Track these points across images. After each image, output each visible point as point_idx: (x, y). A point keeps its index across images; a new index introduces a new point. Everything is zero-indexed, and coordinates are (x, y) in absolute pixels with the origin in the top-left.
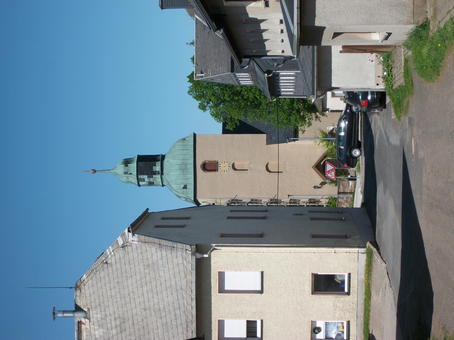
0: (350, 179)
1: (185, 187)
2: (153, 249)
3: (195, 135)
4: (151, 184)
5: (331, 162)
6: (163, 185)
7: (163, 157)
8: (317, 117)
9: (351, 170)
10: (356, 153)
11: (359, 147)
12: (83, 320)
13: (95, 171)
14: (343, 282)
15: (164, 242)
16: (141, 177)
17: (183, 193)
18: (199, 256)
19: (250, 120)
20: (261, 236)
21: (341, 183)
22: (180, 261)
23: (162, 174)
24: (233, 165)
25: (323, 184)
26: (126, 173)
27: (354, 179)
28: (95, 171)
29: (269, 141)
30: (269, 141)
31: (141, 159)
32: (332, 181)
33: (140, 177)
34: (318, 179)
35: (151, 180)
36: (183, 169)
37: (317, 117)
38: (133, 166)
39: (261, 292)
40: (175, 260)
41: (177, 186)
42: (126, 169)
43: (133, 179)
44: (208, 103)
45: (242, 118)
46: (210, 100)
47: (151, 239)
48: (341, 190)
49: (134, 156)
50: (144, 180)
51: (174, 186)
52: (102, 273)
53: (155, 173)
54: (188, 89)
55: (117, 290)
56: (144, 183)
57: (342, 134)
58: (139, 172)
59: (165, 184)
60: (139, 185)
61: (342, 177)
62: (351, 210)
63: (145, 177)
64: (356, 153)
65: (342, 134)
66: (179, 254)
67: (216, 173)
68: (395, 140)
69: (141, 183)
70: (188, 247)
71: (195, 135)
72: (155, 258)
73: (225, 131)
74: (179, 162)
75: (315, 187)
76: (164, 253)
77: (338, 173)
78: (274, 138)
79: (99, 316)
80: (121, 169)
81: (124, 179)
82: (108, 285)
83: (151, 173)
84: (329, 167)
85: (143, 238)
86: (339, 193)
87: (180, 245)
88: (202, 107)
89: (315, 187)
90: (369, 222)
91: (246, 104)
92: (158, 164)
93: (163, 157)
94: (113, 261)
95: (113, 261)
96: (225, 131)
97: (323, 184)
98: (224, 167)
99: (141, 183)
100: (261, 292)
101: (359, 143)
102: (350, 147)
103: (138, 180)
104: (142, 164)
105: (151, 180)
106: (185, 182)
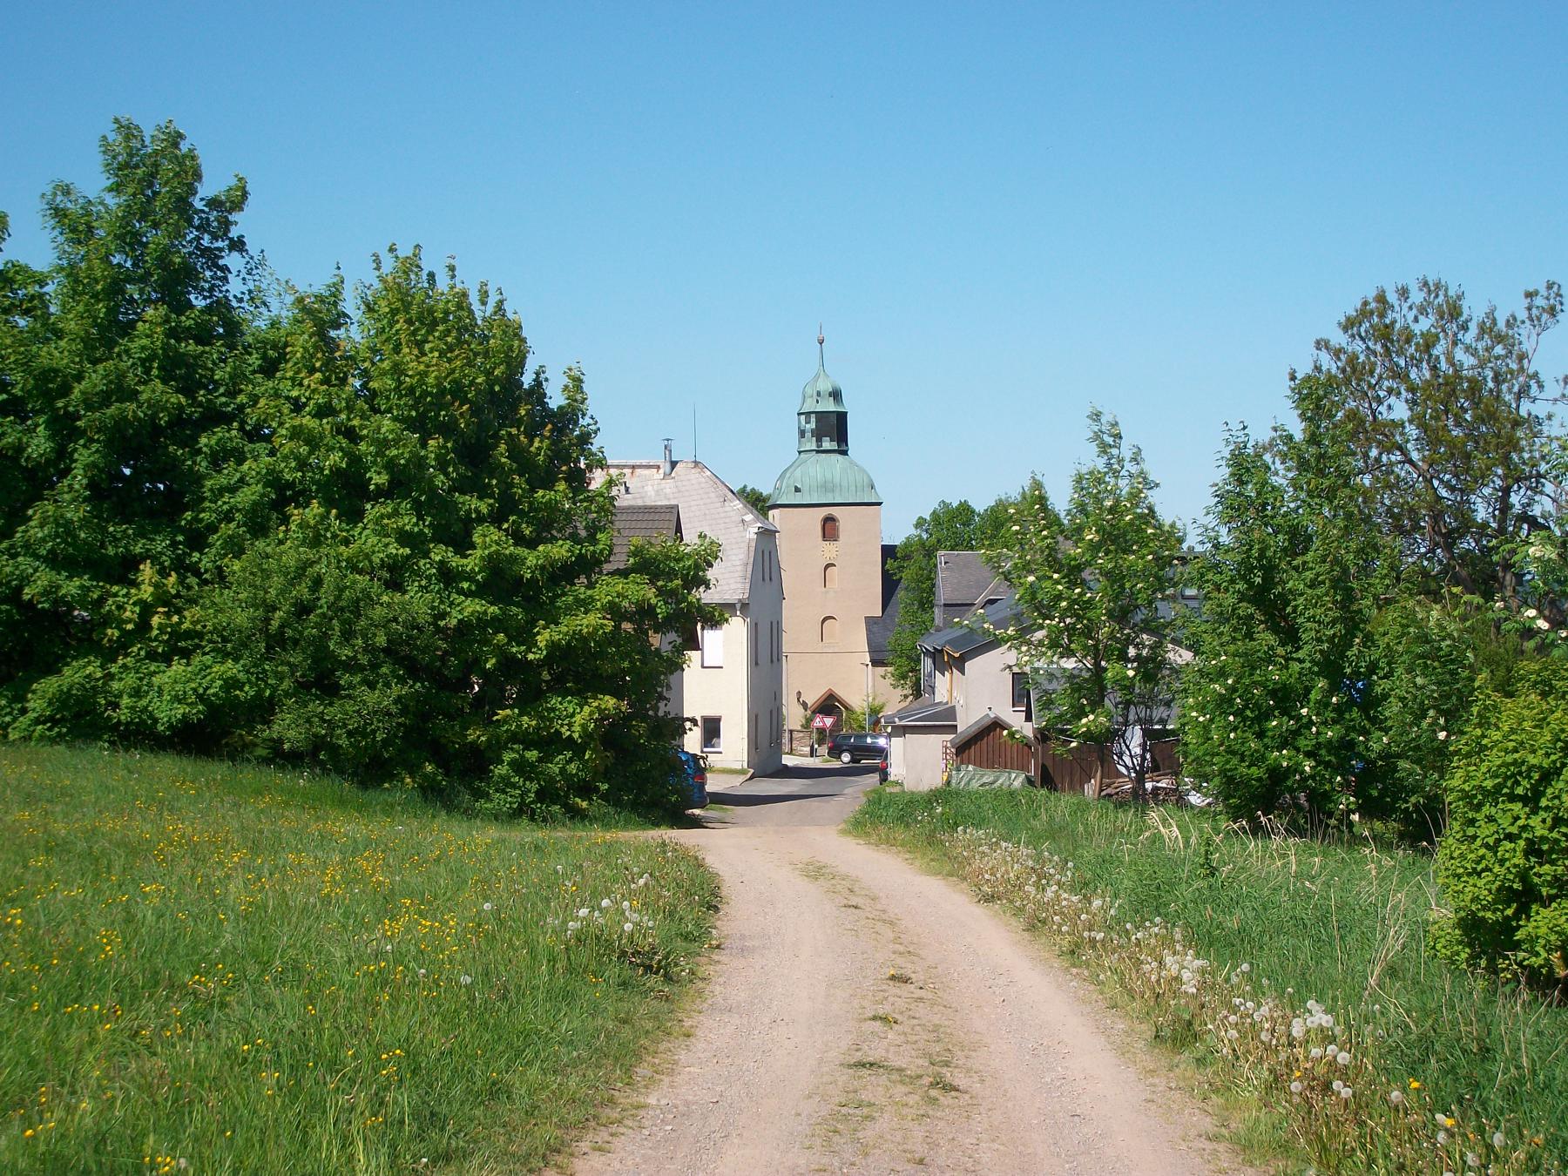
0: (812, 747)
1: (797, 490)
2: (742, 556)
3: (879, 504)
4: (802, 433)
5: (837, 725)
6: (800, 452)
7: (845, 453)
8: (906, 697)
9: (824, 750)
10: (846, 757)
11: (853, 761)
12: (661, 471)
13: (821, 343)
14: (713, 746)
15: (750, 568)
16: (813, 419)
17: (788, 487)
18: (738, 606)
19: (900, 594)
20: (757, 664)
21: (808, 734)
22: (733, 586)
23: (818, 452)
24: (834, 565)
25: (805, 705)
26: (819, 394)
27: (812, 753)
28: (821, 343)
29: (870, 621)
30: (870, 621)
31: (842, 417)
32: (809, 721)
33: (813, 416)
34: (812, 698)
35: (808, 435)
36: (826, 487)
37: (906, 697)
38: (829, 405)
39: (703, 667)
40: (732, 581)
41: (797, 477)
42: (824, 393)
43: (810, 406)
44: (927, 531)
45: (904, 583)
46: (931, 535)
47: (752, 554)
48: (795, 735)
49: (849, 405)
50: (808, 422)
51: (798, 473)
52: (713, 495)
53: (819, 440)
54: (948, 501)
55: (697, 513)
56: (803, 422)
57: (869, 740)
58: (821, 416)
59: (802, 455)
60: (799, 414)
61: (815, 736)
62: (779, 753)
63: (813, 425)
64: (846, 757)
65: (869, 740)
66: (739, 586)
67: (820, 538)
68: (846, 791)
69: (803, 417)
70: (746, 596)
71: (879, 504)
72: (734, 558)
73: (888, 552)
74: (837, 480)
75: (799, 693)
76: (739, 568)
77: (821, 731)
78: (875, 629)
79: (668, 491)
80: (825, 386)
81: (809, 391)
82: (701, 502)
83: (818, 435)
84: (829, 721)
85: (753, 544)
86: (791, 732)
87: (748, 586)
88: (920, 523)
89: (799, 693)
90: (769, 772)
91: (923, 591)
92: (834, 446)
93: (845, 453)
94: (728, 509)
95: (728, 509)
96: (888, 552)
97: (805, 705)
98: (829, 550)
99: (803, 417)
100: (703, 667)
101: (859, 761)
102: (853, 750)
103: (808, 414)
104: (834, 420)
105: (808, 435)
106: (805, 489)
